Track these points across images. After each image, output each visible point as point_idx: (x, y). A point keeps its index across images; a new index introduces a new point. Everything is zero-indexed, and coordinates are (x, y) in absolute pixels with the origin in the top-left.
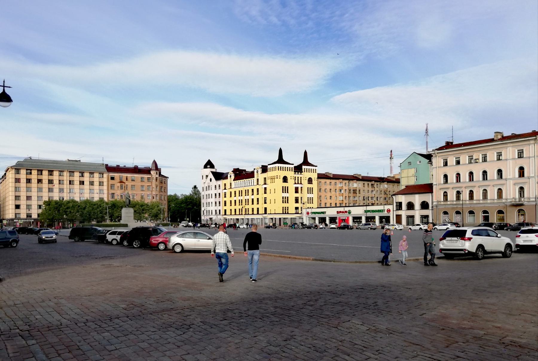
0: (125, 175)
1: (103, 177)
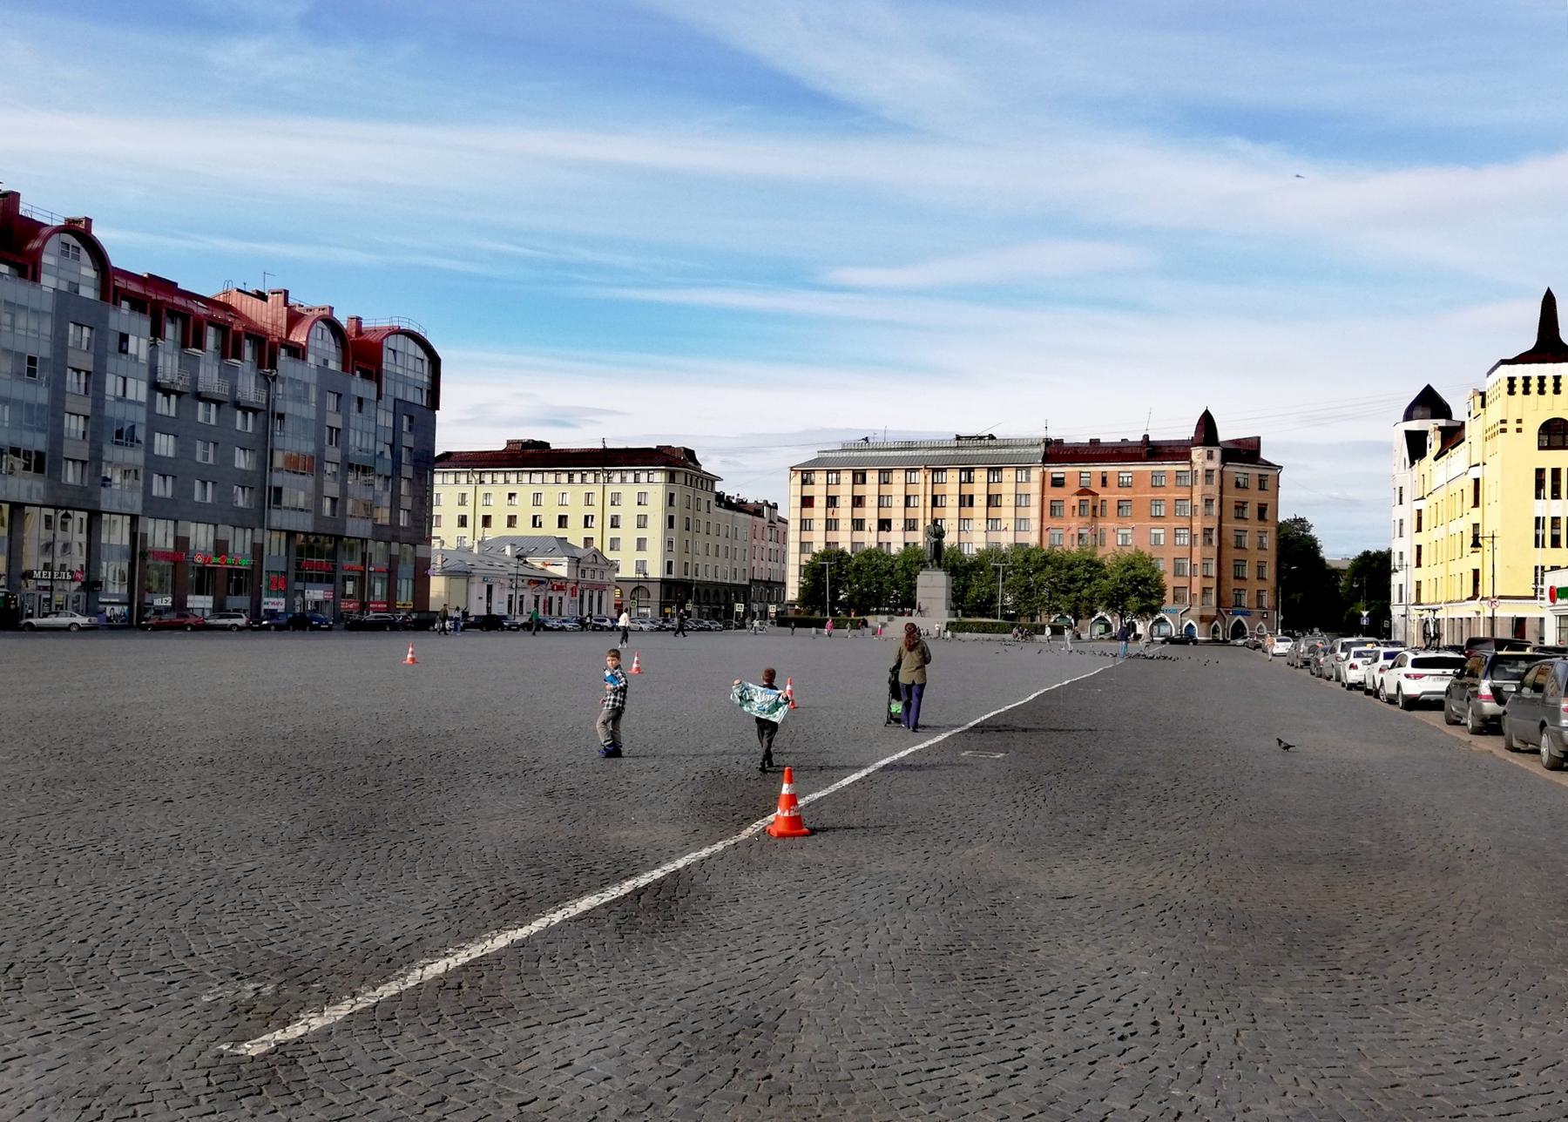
1: (1028, 480)
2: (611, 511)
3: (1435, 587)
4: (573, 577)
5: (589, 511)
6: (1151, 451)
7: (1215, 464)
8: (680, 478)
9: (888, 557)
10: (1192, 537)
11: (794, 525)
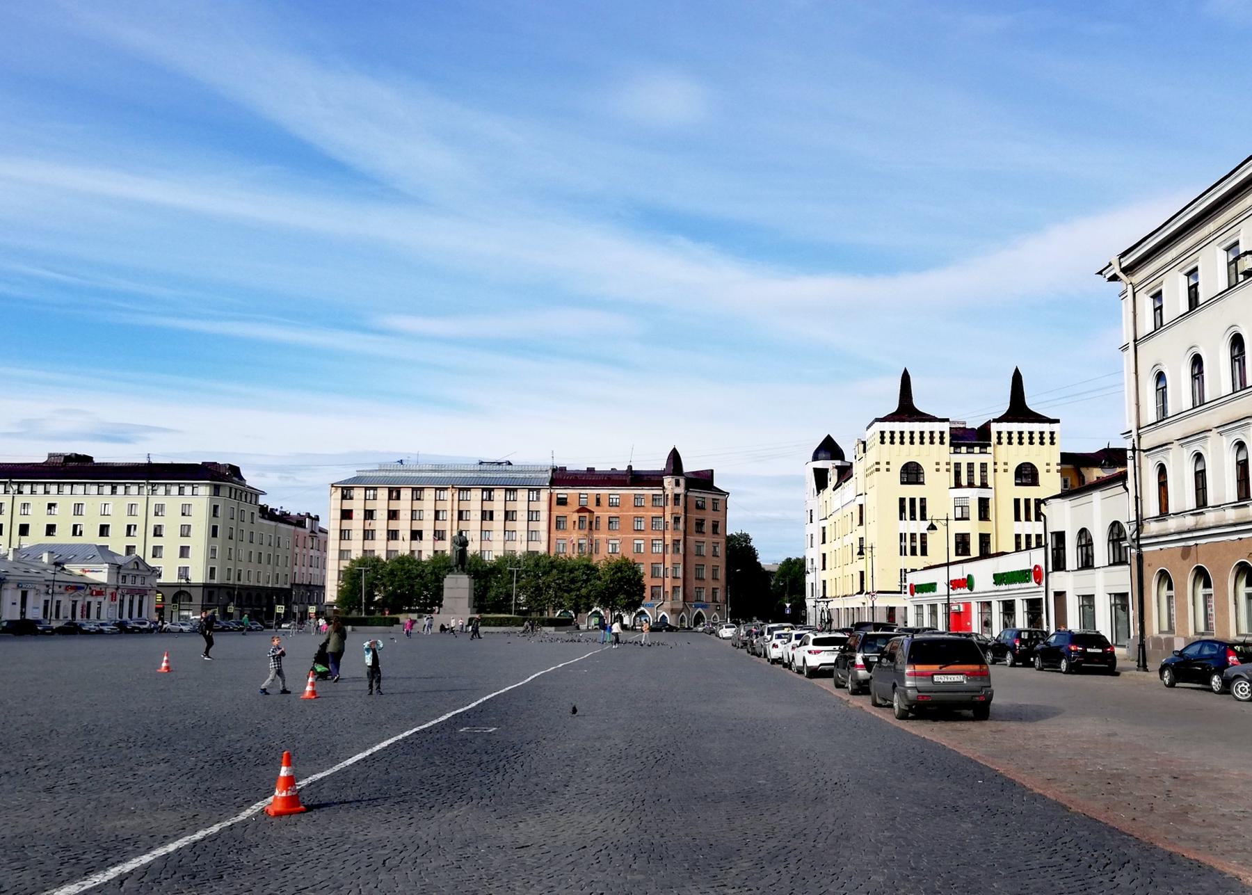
0: (592, 492)
1: (538, 499)
2: (154, 521)
3: (835, 588)
4: (114, 582)
5: (131, 521)
6: (635, 478)
7: (680, 490)
8: (224, 492)
9: (419, 563)
10: (665, 547)
11: (334, 535)
